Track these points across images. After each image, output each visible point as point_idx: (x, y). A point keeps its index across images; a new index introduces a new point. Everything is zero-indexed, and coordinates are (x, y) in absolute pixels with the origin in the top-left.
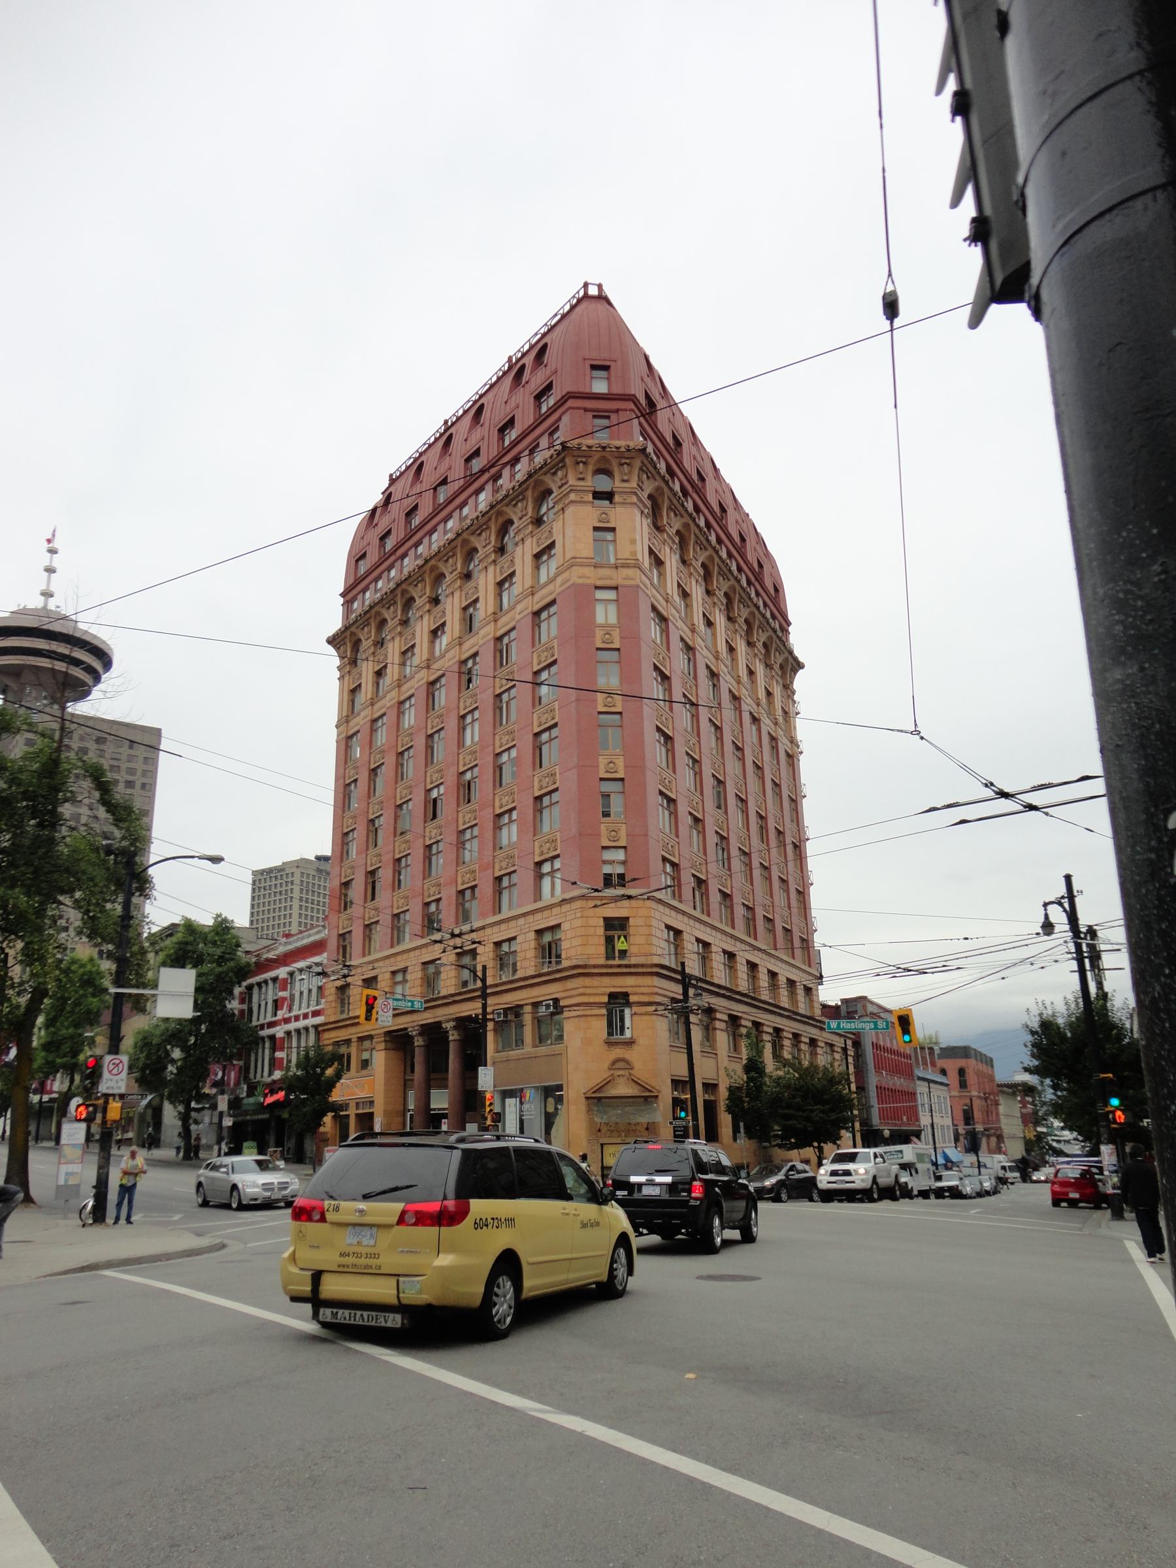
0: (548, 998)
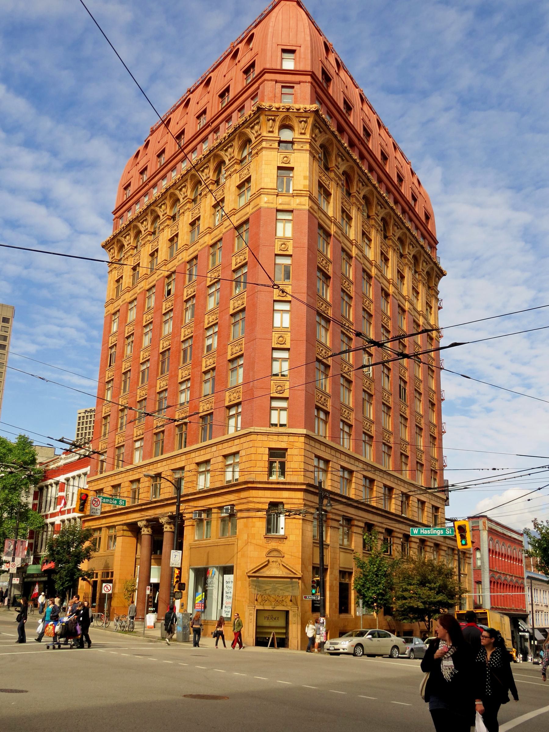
0: (228, 504)
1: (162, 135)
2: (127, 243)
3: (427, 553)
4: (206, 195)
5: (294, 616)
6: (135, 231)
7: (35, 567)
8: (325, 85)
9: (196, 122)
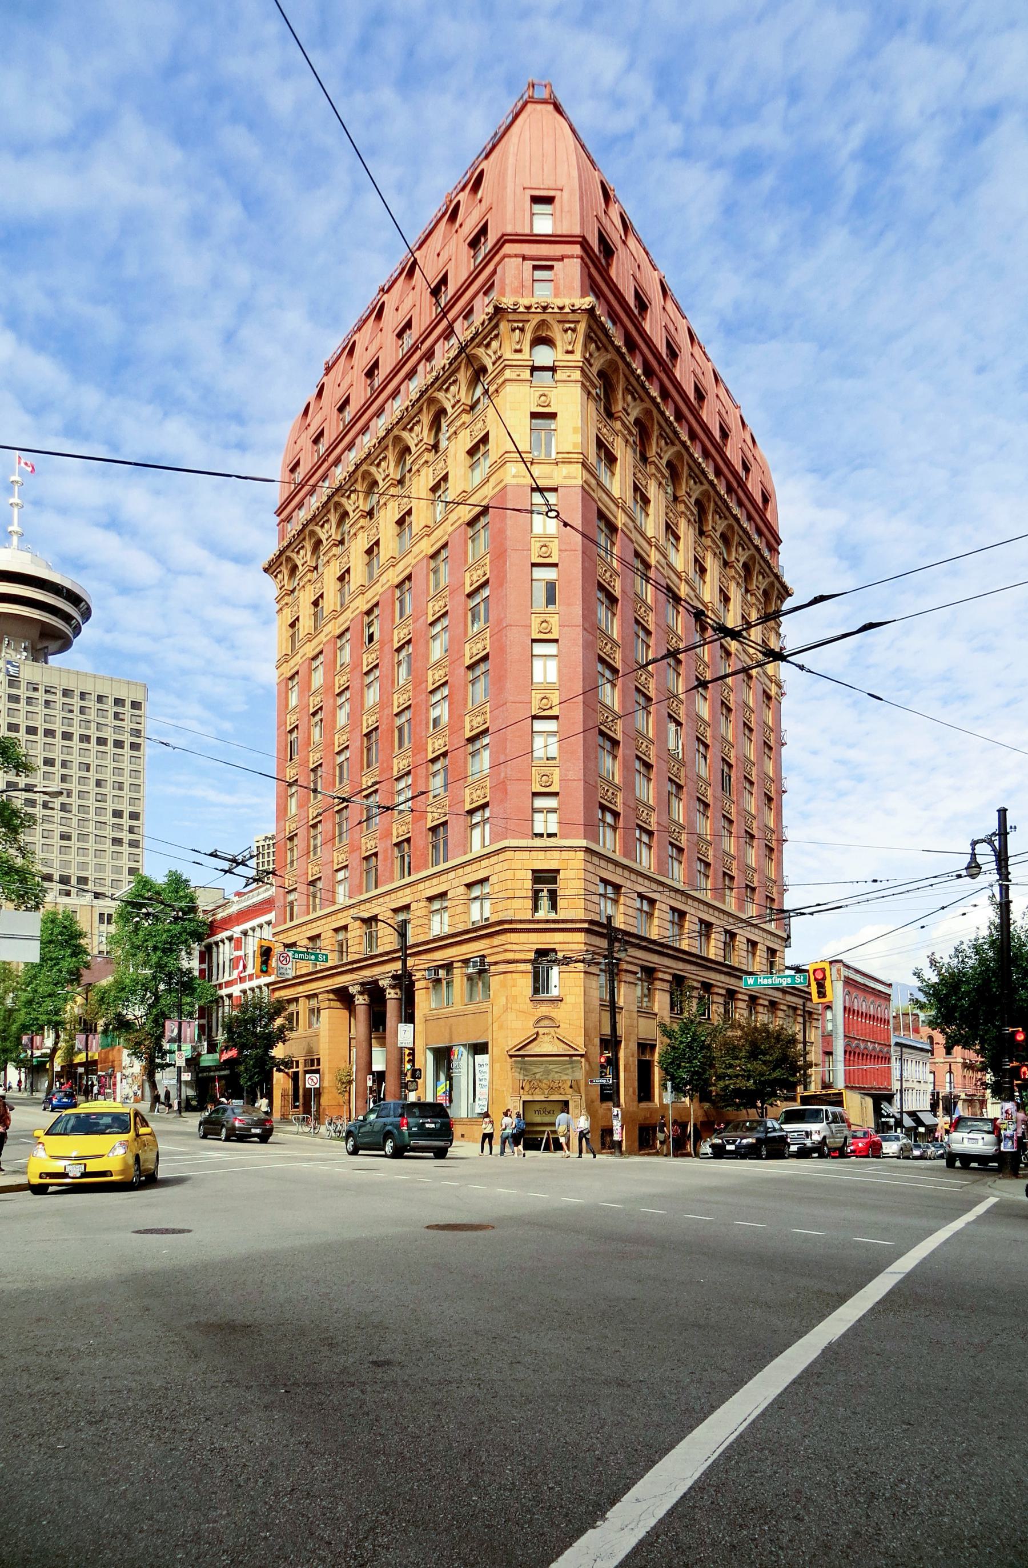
1: (343, 373)
2: (302, 561)
3: (759, 1015)
4: (418, 471)
5: (576, 1107)
6: (313, 541)
7: (211, 1056)
8: (603, 261)
9: (397, 343)
